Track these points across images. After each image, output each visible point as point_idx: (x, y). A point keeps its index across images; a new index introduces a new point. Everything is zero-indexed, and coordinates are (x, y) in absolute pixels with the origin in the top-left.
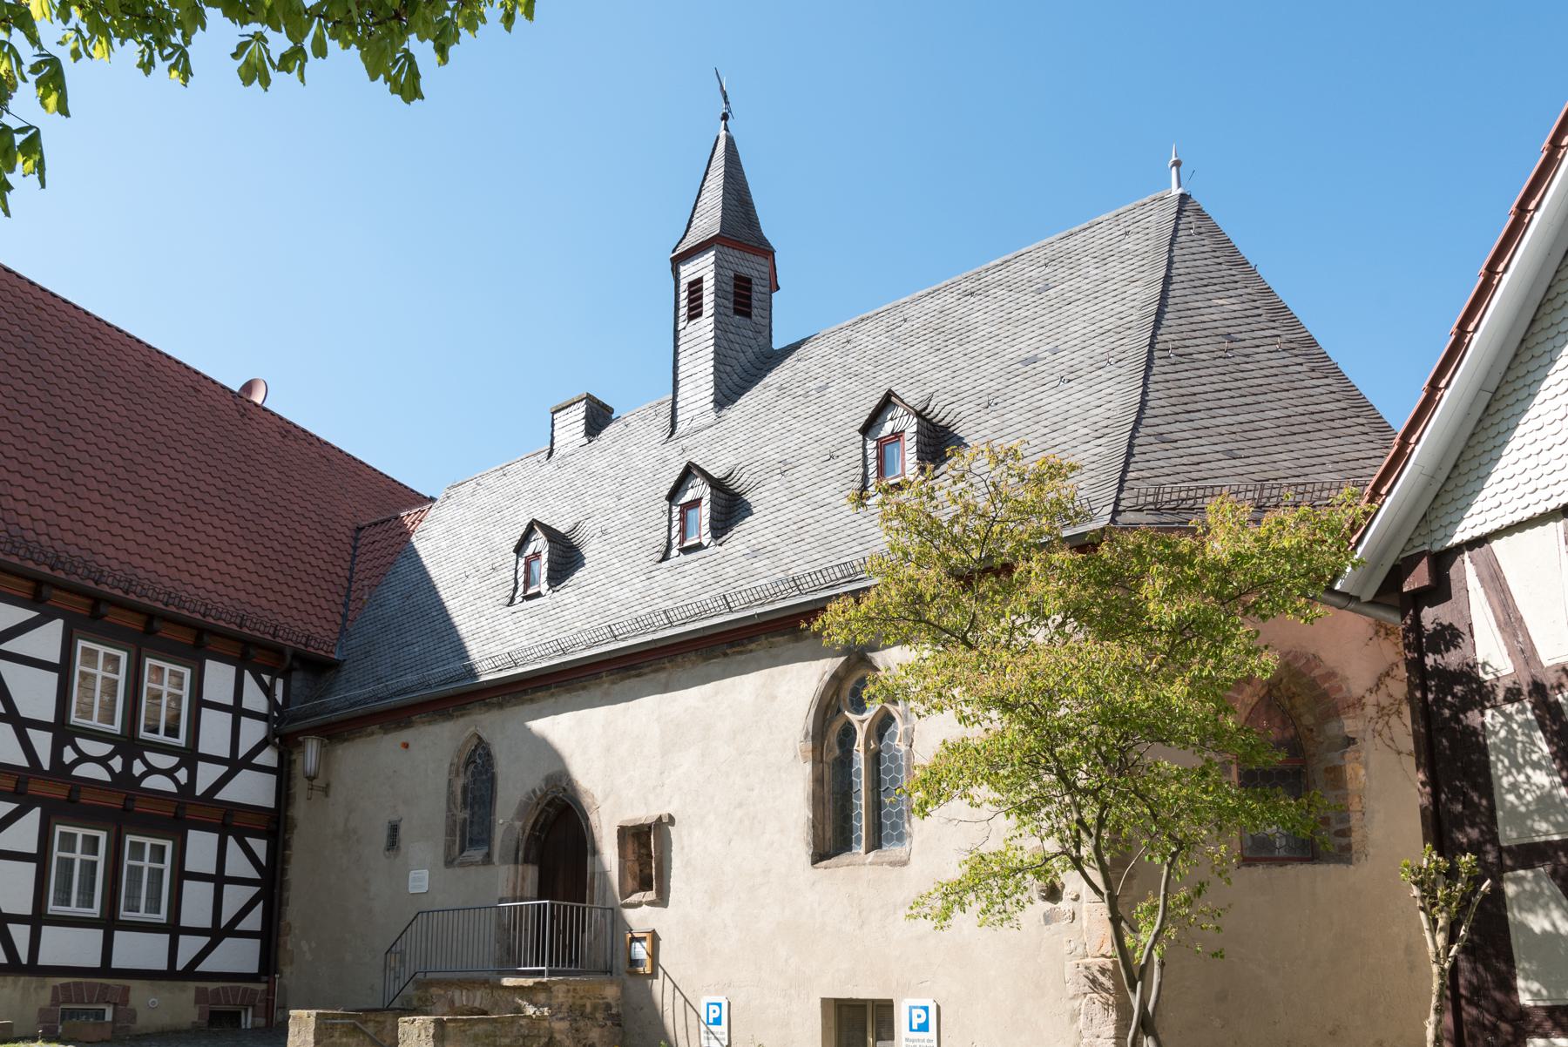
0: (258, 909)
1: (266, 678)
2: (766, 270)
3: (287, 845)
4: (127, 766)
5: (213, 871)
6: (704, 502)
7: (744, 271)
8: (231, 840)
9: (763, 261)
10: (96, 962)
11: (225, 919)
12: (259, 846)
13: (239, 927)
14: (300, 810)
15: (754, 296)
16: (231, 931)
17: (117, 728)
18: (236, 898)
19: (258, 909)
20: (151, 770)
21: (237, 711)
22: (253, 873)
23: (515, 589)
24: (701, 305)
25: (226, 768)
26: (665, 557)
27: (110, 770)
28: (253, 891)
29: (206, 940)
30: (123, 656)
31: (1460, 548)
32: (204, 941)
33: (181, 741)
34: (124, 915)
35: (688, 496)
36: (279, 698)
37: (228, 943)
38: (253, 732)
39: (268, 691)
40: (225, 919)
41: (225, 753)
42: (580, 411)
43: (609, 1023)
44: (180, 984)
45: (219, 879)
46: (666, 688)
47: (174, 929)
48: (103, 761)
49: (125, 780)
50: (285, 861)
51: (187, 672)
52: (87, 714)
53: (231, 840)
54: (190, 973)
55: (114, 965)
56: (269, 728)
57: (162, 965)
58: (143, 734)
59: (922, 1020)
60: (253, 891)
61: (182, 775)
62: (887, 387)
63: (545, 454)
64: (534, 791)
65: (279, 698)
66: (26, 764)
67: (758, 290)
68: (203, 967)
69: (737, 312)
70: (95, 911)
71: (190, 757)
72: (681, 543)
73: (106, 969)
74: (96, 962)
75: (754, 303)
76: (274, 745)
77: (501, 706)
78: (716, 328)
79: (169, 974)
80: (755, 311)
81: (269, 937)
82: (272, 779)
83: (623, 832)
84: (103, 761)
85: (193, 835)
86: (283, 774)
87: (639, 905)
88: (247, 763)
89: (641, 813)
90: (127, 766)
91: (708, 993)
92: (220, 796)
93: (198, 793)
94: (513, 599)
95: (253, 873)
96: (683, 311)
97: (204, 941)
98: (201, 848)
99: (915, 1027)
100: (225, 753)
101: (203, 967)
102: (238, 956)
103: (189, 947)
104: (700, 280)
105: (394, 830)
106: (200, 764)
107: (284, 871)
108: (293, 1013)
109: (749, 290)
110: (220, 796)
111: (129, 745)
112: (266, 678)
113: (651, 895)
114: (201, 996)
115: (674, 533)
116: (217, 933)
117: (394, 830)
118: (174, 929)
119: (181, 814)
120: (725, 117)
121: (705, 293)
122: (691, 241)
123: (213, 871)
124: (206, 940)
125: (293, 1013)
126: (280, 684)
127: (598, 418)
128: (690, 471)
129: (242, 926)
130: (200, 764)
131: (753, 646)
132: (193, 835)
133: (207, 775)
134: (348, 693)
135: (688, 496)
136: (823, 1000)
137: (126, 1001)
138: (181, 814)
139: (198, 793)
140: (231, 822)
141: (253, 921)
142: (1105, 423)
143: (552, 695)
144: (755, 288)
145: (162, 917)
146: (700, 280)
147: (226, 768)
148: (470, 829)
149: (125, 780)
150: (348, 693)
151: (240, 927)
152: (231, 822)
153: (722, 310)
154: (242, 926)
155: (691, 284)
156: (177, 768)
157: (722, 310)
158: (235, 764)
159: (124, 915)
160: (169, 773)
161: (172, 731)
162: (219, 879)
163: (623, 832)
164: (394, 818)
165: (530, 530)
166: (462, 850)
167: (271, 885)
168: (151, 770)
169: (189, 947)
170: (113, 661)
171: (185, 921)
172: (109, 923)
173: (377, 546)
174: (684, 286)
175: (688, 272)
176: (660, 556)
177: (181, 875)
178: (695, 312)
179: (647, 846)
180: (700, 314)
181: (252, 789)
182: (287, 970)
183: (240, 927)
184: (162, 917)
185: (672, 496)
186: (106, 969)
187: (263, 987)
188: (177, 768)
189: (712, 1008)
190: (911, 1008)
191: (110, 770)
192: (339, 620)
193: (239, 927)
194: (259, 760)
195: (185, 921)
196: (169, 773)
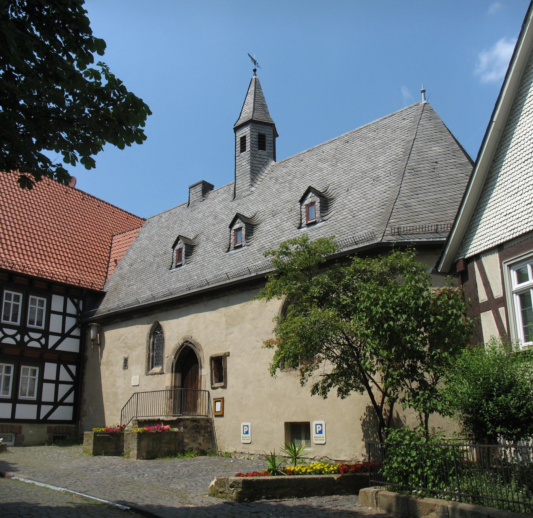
0: (73, 394)
1: (76, 300)
2: (272, 131)
3: (84, 368)
4: (22, 338)
5: (55, 379)
6: (243, 229)
7: (263, 132)
8: (62, 367)
9: (270, 128)
10: (9, 416)
11: (59, 398)
12: (73, 368)
13: (64, 402)
14: (89, 353)
15: (267, 142)
16: (61, 403)
17: (18, 323)
18: (63, 389)
19: (73, 394)
20: (31, 339)
21: (64, 314)
22: (70, 379)
23: (172, 263)
24: (245, 147)
25: (60, 337)
26: (228, 251)
27: (16, 340)
28: (70, 387)
29: (52, 407)
30: (21, 295)
31: (477, 257)
32: (51, 407)
33: (43, 327)
34: (20, 397)
35: (236, 226)
36: (81, 308)
37: (60, 408)
38: (70, 322)
39: (77, 306)
40: (59, 398)
41: (60, 331)
42: (199, 188)
43: (206, 435)
44: (41, 425)
45: (57, 382)
46: (228, 304)
47: (39, 402)
48: (13, 337)
49: (21, 344)
50: (83, 374)
51: (45, 300)
52: (6, 318)
53: (62, 367)
54: (45, 420)
55: (16, 418)
56: (77, 321)
57: (34, 417)
58: (29, 325)
59: (320, 429)
60: (70, 387)
61: (43, 341)
62: (309, 185)
63: (187, 205)
64: (179, 344)
65: (81, 308)
66: (72, 386)
67: (269, 139)
68: (51, 418)
69: (260, 149)
70: (9, 396)
71: (46, 333)
72: (235, 244)
73: (13, 419)
74: (9, 416)
75: (267, 144)
76: (79, 327)
77: (166, 310)
78: (251, 156)
79: (38, 421)
80: (267, 148)
81: (77, 405)
82: (77, 341)
83: (212, 359)
84: (13, 337)
85: (47, 365)
86: (83, 339)
87: (217, 388)
88: (68, 335)
89: (219, 352)
90: (22, 338)
91: (243, 421)
92: (57, 349)
93: (49, 347)
94: (172, 266)
95: (70, 379)
96: (239, 149)
97: (51, 407)
98: (50, 370)
99: (318, 432)
100: (60, 331)
101: (51, 418)
102: (64, 413)
103: (45, 410)
104: (245, 137)
105: (126, 360)
106: (50, 336)
107: (82, 378)
108: (86, 433)
109: (265, 139)
110: (57, 349)
111: (23, 330)
112: (76, 300)
113: (222, 384)
114: (49, 431)
115: (232, 241)
116: (56, 404)
117: (126, 360)
118: (39, 402)
119: (41, 357)
120: (255, 70)
121: (247, 145)
122: (240, 122)
123: (55, 379)
124: (52, 407)
125: (86, 433)
126: (81, 302)
127: (207, 188)
128: (238, 216)
129: (66, 401)
130: (50, 336)
131: (259, 286)
132: (47, 365)
133: (53, 340)
134: (106, 307)
135: (236, 226)
136: (285, 423)
137: (20, 433)
138: (41, 357)
139: (49, 347)
140: (62, 359)
141: (70, 399)
142: (386, 200)
143: (185, 306)
144: (267, 138)
145: (34, 398)
146: (245, 137)
147: (60, 337)
148: (154, 358)
149: (21, 344)
150: (106, 307)
151: (65, 401)
152: (62, 359)
153: (254, 149)
154: (66, 401)
155: (241, 138)
156: (41, 338)
157: (254, 149)
158: (64, 335)
159: (20, 397)
160: (38, 340)
161: (39, 324)
162: (57, 382)
163: (212, 359)
164: (126, 356)
165: (178, 239)
166: (152, 368)
167: (78, 384)
168: (31, 339)
169: (45, 410)
170: (17, 298)
171: (44, 399)
172: (14, 401)
173: (120, 243)
174: (238, 140)
175: (240, 134)
176: (227, 250)
177: (42, 381)
178: (243, 149)
179: (219, 364)
180: (245, 150)
181: (70, 345)
182: (84, 419)
183: (65, 401)
184: (34, 398)
185: (231, 226)
186: (13, 419)
187: (74, 426)
188: (41, 338)
189: (245, 427)
190: (316, 425)
191: (16, 340)
192: (106, 263)
193: (64, 402)
194: (73, 333)
195: (44, 399)
196: (38, 340)
